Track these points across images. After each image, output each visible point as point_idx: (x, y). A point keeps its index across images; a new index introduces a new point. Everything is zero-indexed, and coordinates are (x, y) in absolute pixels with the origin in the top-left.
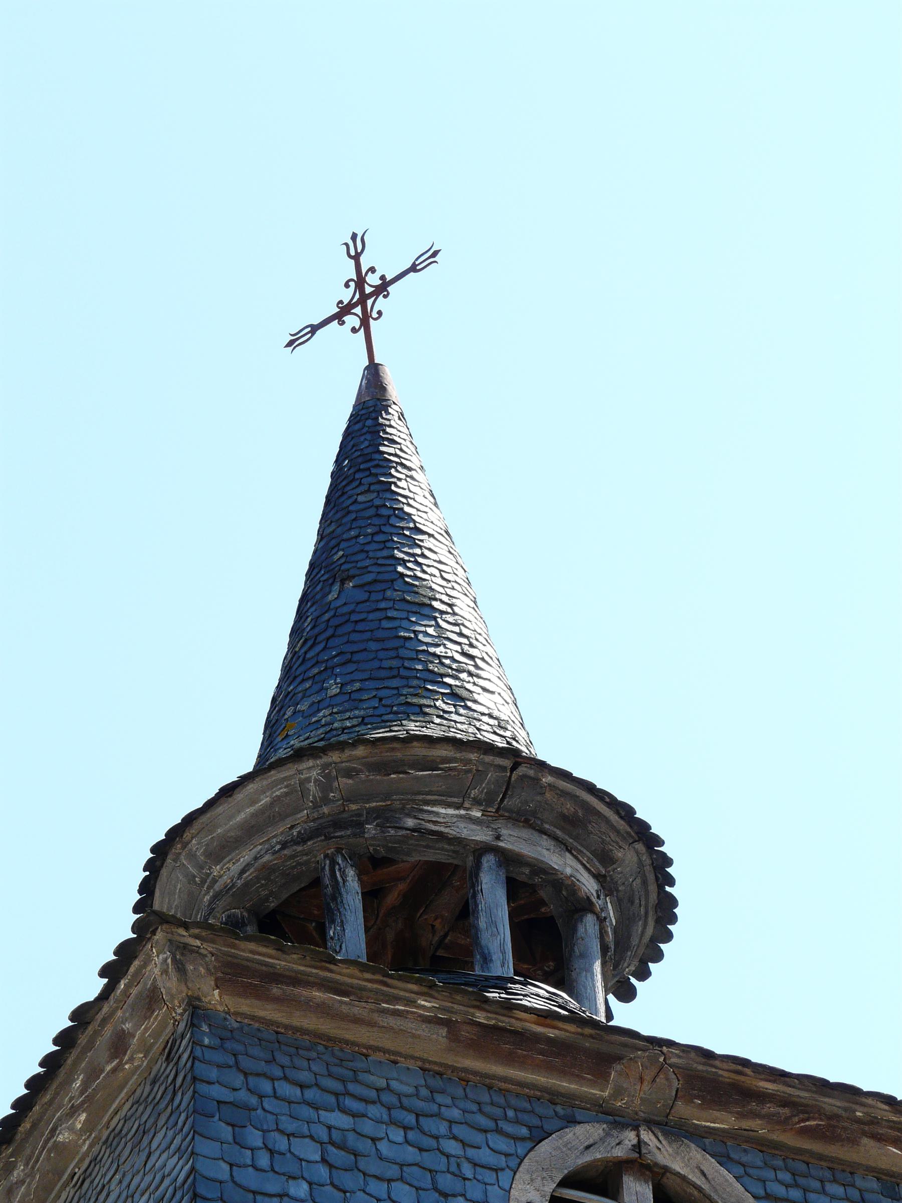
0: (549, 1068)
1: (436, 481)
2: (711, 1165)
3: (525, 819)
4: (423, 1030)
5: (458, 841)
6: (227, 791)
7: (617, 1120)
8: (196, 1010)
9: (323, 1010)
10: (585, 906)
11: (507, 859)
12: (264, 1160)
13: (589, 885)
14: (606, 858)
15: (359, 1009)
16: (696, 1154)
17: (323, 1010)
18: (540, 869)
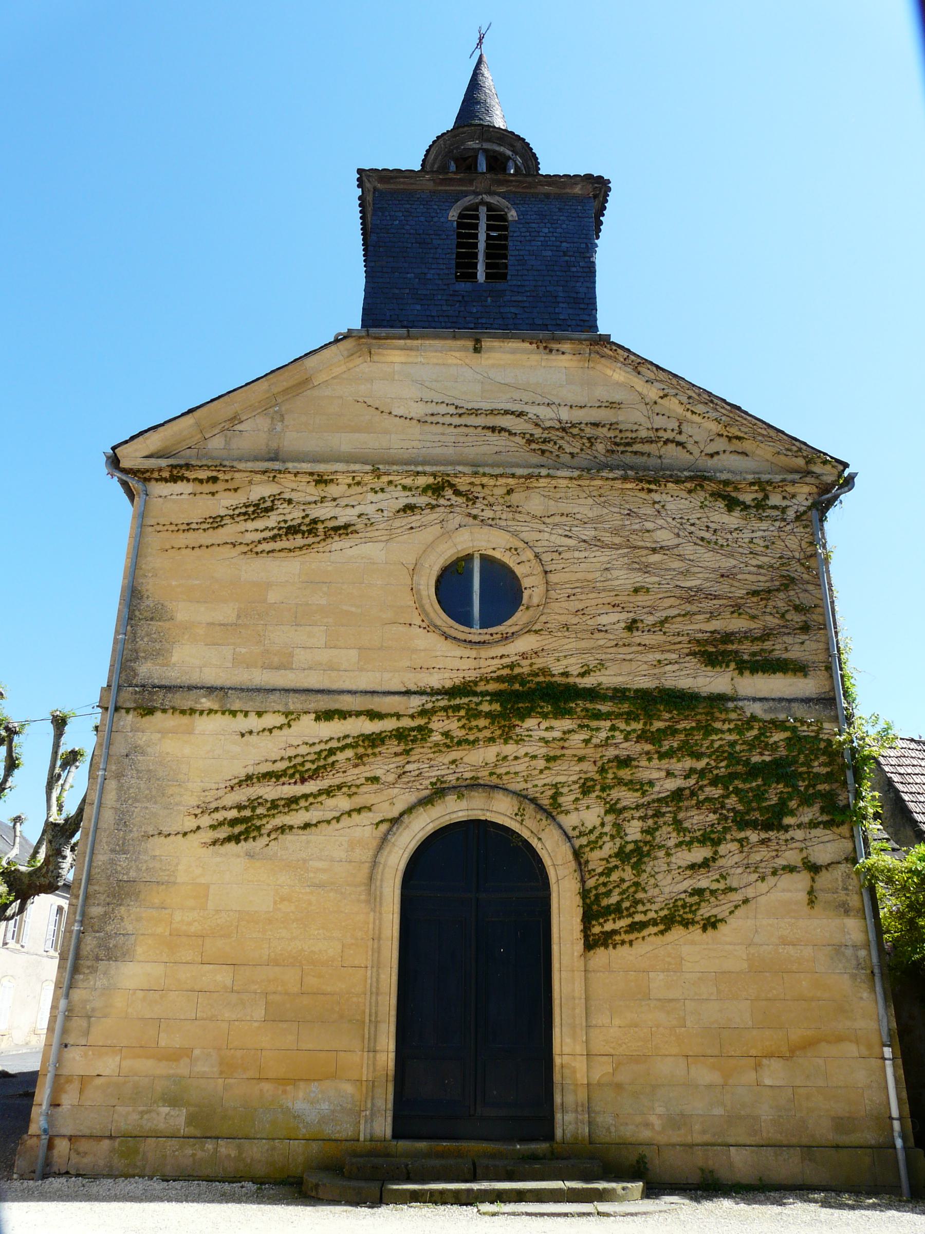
0: (459, 185)
1: (489, 78)
2: (500, 199)
3: (489, 140)
4: (428, 183)
5: (473, 149)
6: (428, 151)
7: (477, 194)
8: (375, 189)
9: (404, 183)
10: (509, 158)
11: (485, 151)
12: (388, 218)
13: (509, 153)
14: (512, 146)
15: (412, 181)
16: (497, 198)
17: (404, 183)
18: (495, 151)
